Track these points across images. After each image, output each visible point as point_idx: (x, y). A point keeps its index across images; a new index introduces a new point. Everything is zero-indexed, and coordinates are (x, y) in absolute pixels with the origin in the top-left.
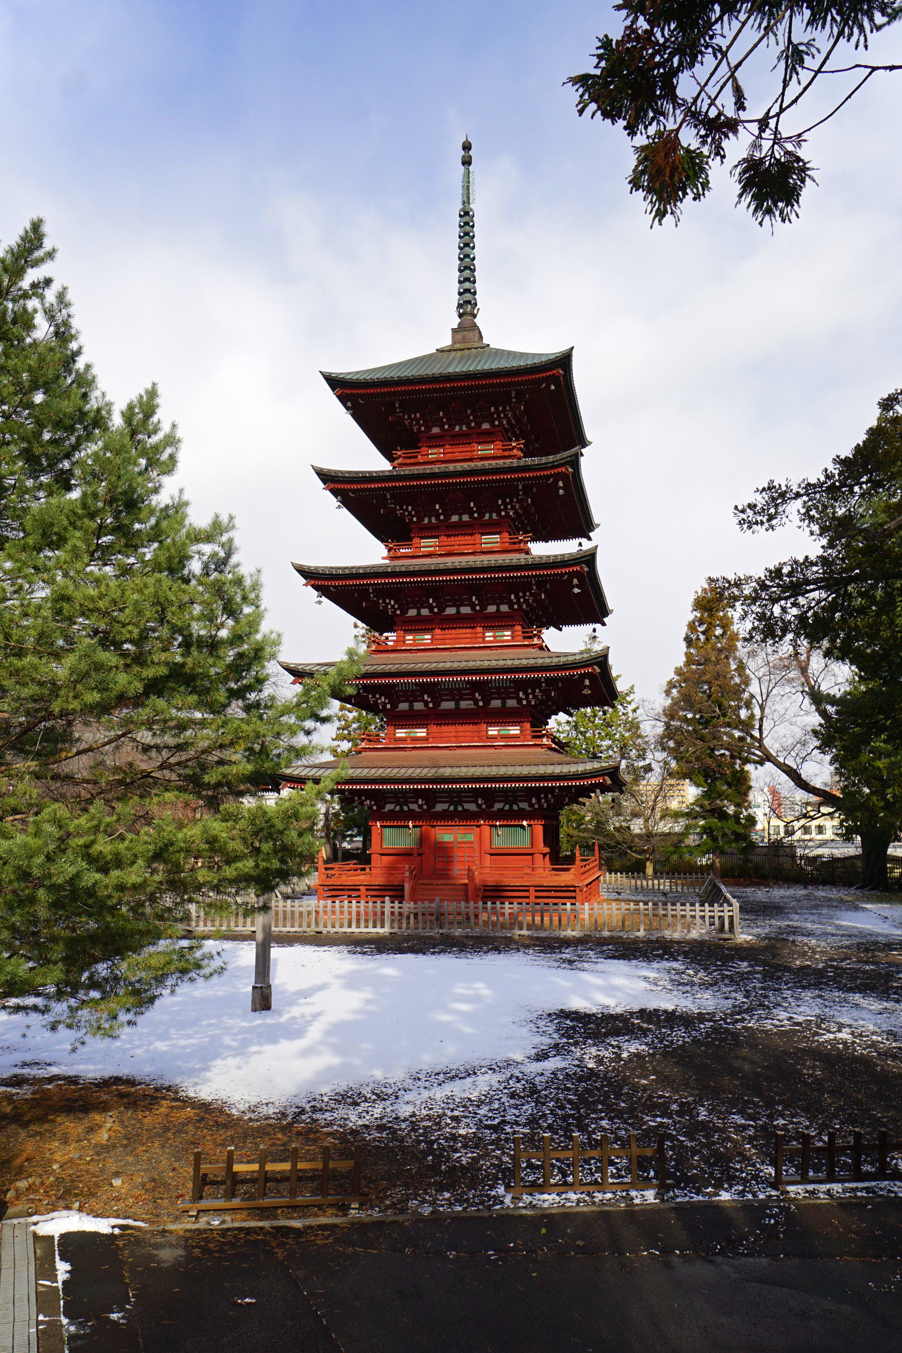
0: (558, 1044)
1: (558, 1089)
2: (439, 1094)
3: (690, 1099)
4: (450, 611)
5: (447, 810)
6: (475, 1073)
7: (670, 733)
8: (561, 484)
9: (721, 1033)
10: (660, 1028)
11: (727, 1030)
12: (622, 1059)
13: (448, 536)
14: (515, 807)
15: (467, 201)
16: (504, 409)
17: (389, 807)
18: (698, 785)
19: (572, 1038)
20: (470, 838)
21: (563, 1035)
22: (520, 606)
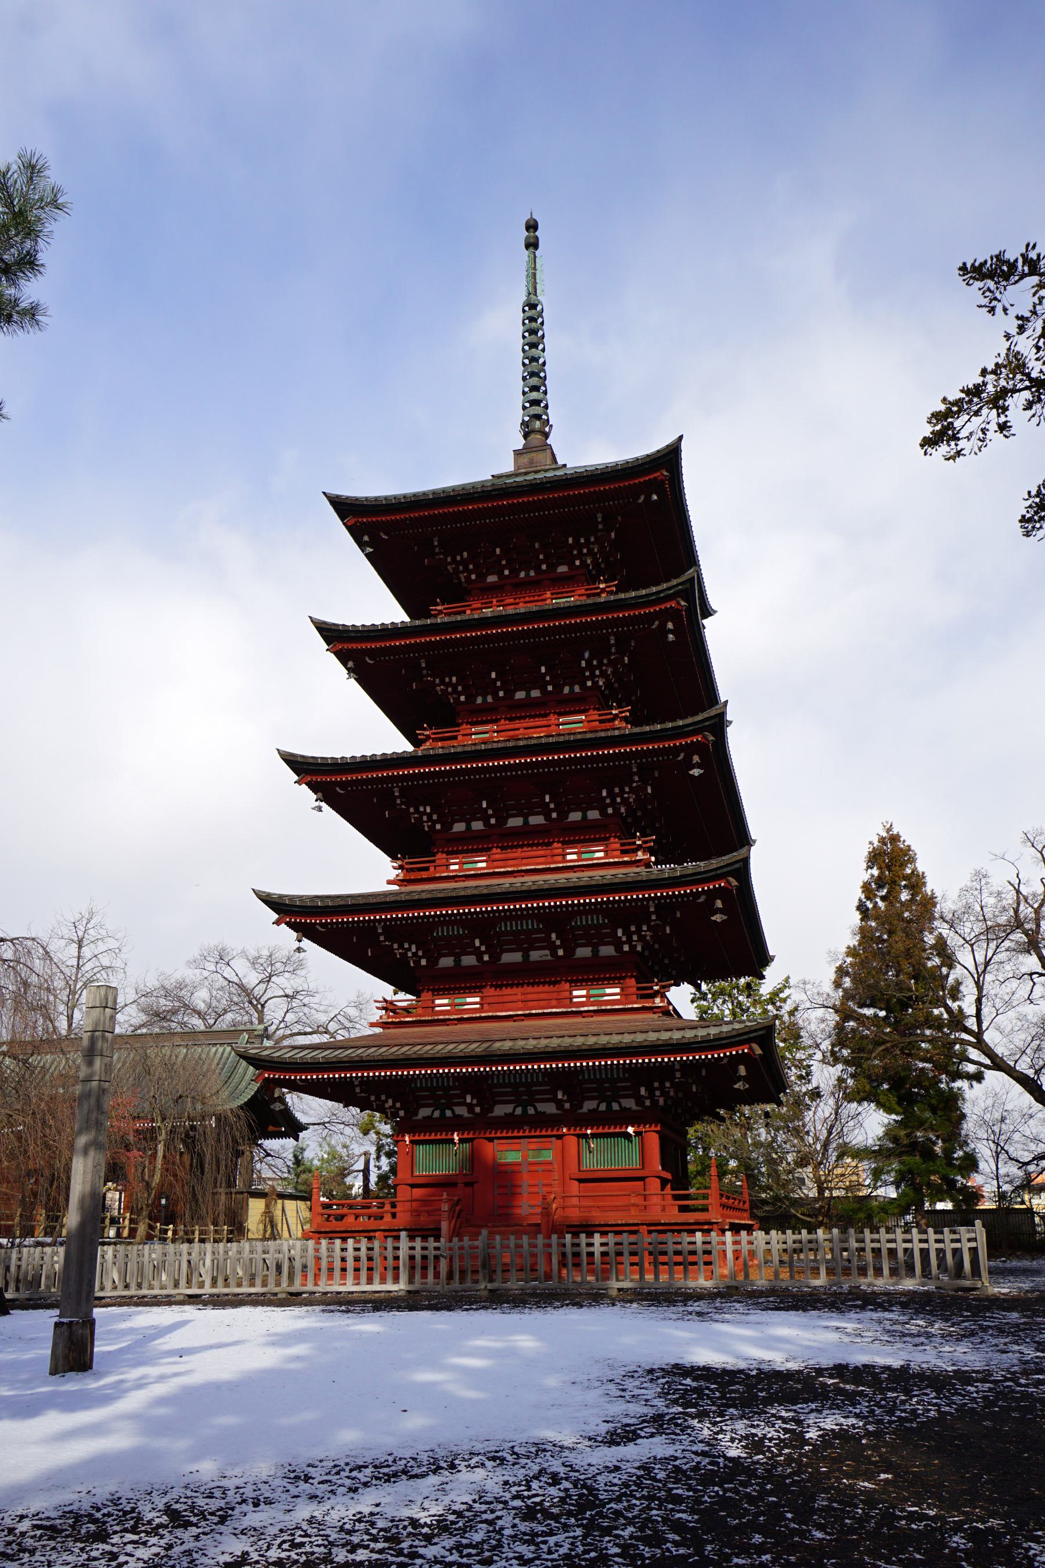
0: (661, 1416)
1: (651, 1498)
2: (341, 1510)
3: (994, 1522)
4: (515, 822)
5: (512, 1114)
6: (452, 1466)
7: (841, 1037)
8: (670, 625)
9: (1014, 1399)
10: (883, 1391)
11: (1026, 1396)
12: (807, 1442)
13: (511, 719)
14: (615, 1107)
15: (533, 291)
16: (587, 540)
17: (424, 1112)
18: (889, 1111)
19: (695, 1406)
20: (548, 1156)
21: (675, 1402)
22: (616, 810)
